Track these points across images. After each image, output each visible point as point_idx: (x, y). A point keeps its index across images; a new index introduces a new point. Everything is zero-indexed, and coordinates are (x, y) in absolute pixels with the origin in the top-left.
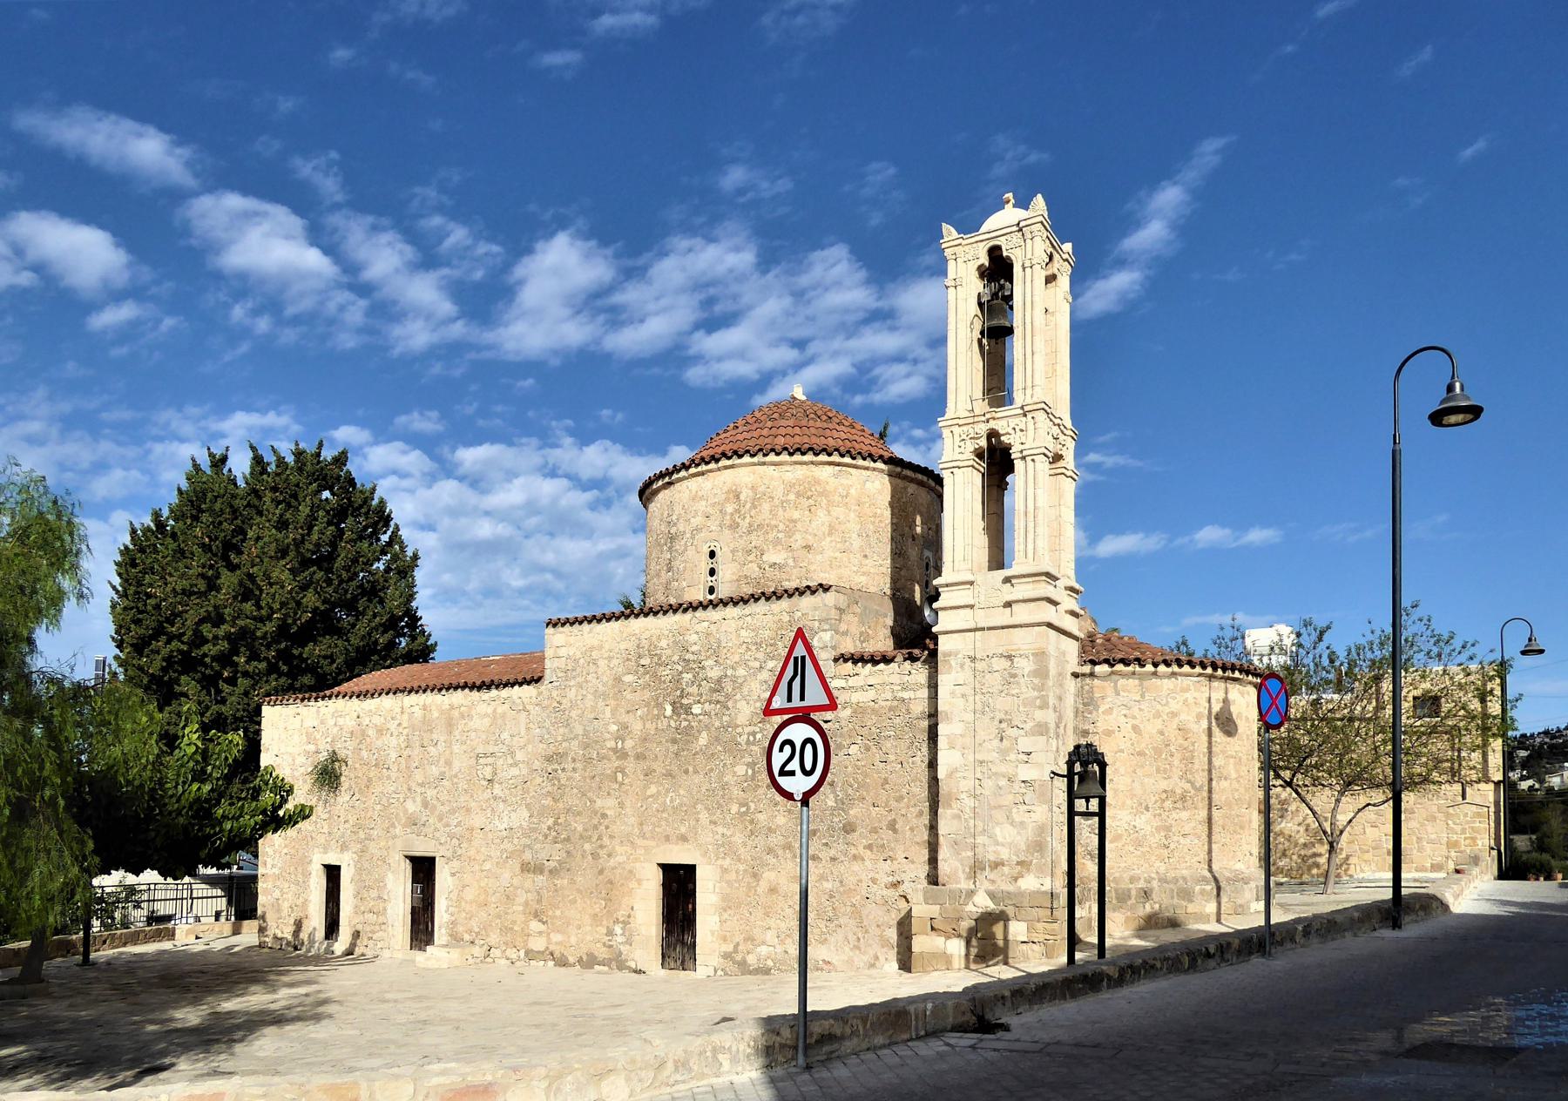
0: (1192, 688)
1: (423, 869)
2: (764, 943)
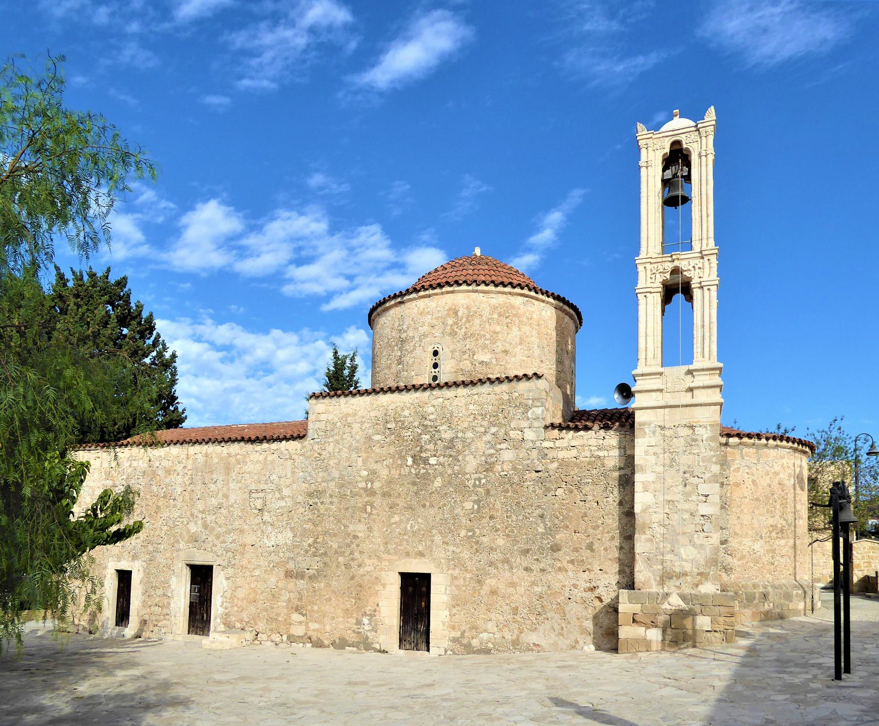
2: (485, 631)
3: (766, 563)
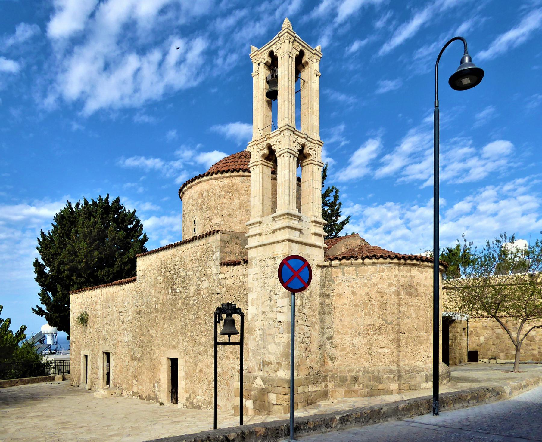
0: (386, 270)
2: (198, 395)
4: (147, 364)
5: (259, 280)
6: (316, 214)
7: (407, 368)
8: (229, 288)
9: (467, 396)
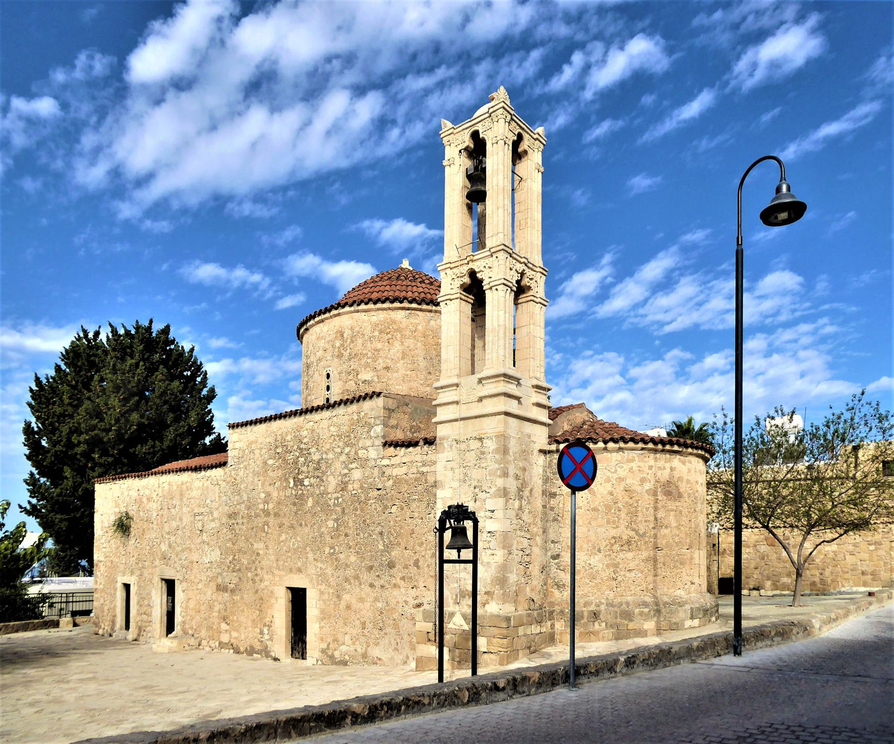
0: (637, 459)
1: (170, 585)
2: (344, 644)
3: (605, 578)
4: (249, 597)
5: (456, 471)
6: (538, 375)
7: (666, 599)
8: (398, 481)
9: (770, 632)
